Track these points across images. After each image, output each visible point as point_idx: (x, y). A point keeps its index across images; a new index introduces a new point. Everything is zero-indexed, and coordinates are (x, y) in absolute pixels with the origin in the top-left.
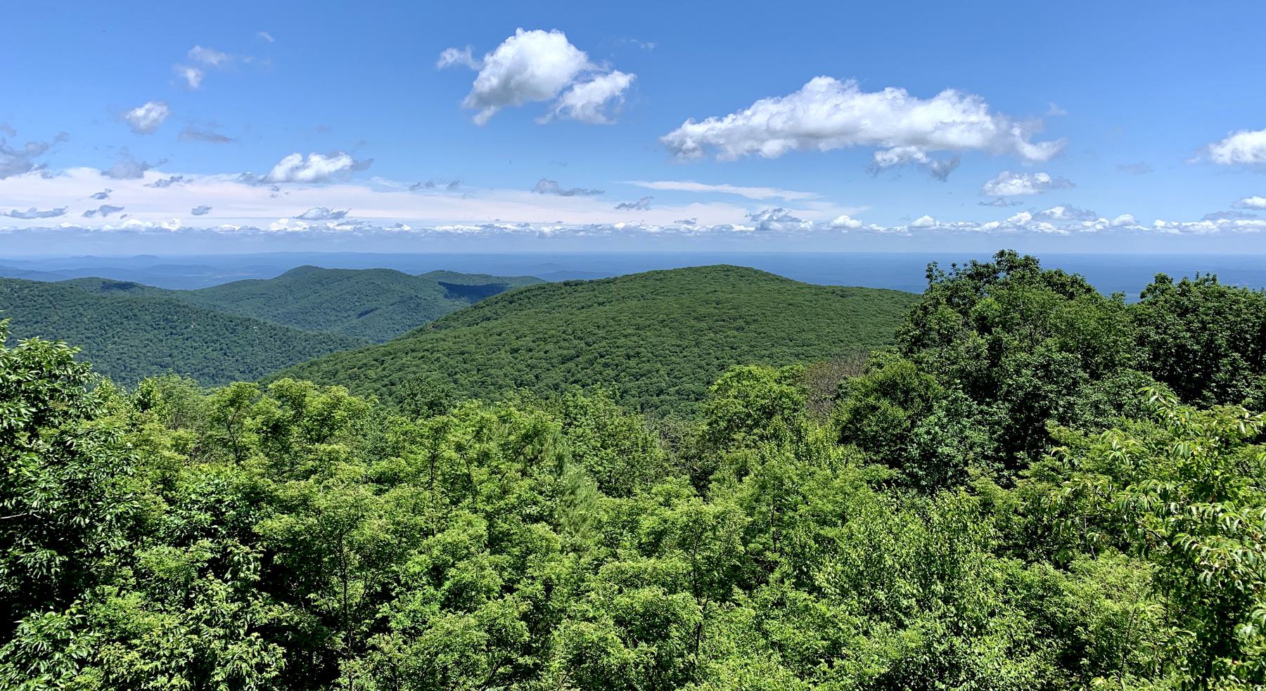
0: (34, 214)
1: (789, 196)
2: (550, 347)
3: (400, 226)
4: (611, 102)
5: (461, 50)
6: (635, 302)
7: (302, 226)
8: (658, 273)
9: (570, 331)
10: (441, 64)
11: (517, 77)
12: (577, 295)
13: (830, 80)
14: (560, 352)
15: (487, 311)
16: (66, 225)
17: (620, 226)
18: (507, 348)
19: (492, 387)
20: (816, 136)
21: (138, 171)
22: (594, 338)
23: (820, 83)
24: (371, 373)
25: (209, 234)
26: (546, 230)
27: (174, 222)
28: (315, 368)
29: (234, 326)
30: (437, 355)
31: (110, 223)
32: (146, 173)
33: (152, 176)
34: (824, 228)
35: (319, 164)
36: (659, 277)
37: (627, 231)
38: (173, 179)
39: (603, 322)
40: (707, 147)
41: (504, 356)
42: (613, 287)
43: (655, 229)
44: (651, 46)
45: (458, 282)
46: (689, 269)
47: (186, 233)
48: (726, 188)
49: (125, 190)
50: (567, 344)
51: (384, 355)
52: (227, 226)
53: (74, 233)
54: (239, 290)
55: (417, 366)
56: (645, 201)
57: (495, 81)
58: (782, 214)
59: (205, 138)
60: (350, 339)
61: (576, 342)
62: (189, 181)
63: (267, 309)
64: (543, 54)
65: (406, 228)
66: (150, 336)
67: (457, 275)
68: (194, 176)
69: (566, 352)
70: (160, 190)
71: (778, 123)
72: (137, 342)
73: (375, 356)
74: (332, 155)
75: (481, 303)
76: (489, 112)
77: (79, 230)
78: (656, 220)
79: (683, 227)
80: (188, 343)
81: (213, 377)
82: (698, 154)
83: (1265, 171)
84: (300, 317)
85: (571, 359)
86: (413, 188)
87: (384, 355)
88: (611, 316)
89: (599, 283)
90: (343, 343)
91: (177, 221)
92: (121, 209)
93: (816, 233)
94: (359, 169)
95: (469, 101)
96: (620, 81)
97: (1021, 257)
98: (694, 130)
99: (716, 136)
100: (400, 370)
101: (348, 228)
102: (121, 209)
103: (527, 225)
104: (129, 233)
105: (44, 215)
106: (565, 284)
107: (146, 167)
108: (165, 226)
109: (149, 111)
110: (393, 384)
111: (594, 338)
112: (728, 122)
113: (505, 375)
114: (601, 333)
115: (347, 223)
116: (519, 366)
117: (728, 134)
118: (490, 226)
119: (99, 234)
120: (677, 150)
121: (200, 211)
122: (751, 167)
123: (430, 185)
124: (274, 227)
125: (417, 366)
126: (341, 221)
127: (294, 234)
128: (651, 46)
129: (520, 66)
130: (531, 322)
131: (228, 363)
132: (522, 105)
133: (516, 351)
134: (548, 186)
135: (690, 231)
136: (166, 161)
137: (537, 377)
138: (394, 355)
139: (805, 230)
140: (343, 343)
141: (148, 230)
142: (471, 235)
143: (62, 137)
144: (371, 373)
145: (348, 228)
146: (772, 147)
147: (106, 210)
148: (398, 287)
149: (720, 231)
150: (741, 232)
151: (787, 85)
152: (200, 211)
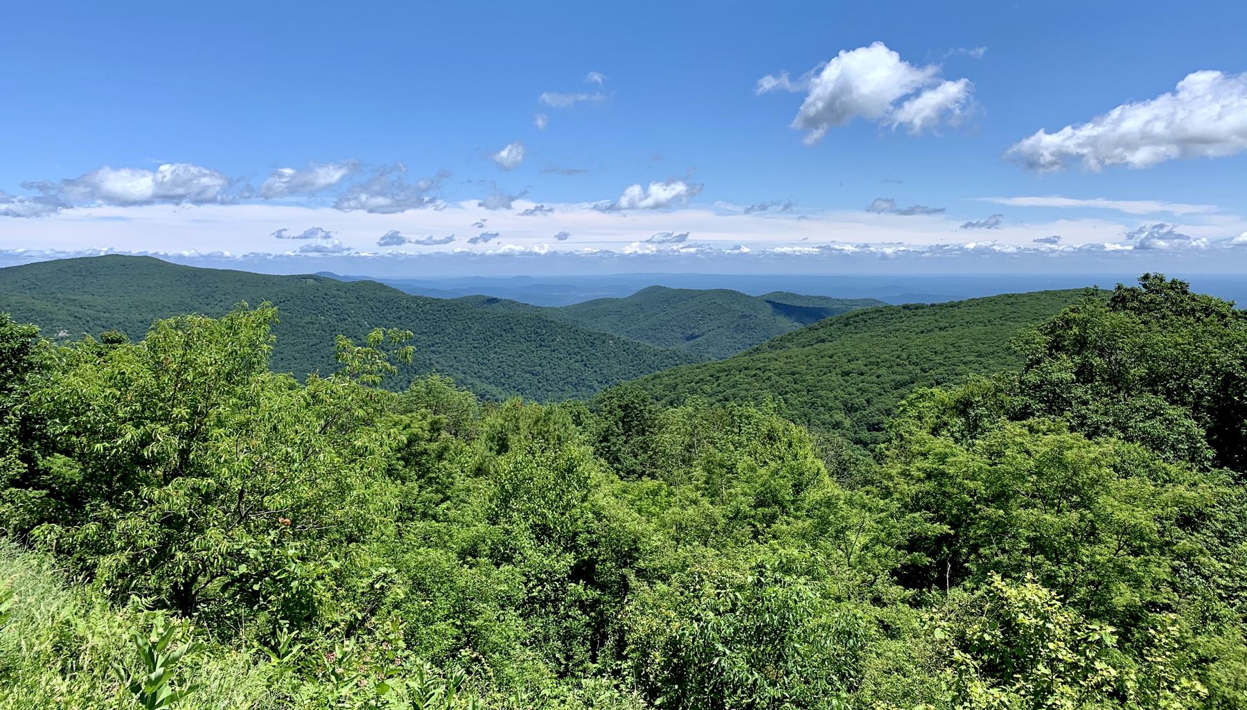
0: (430, 242)
1: (1180, 209)
2: (882, 371)
3: (738, 247)
4: (944, 113)
5: (776, 75)
6: (981, 327)
7: (652, 249)
8: (1009, 296)
9: (905, 356)
10: (760, 90)
11: (843, 99)
12: (916, 318)
13: (1217, 74)
14: (893, 377)
15: (821, 333)
16: (458, 250)
17: (971, 246)
18: (838, 370)
19: (822, 409)
20: (1204, 141)
21: (507, 203)
22: (930, 364)
23: (1200, 81)
24: (707, 388)
25: (571, 258)
26: (888, 251)
27: (543, 247)
28: (658, 381)
29: (594, 340)
30: (768, 374)
31: (490, 248)
32: (513, 204)
33: (521, 205)
34: (1224, 245)
35: (659, 192)
36: (1011, 300)
37: (979, 252)
38: (537, 209)
39: (940, 348)
40: (1065, 159)
41: (835, 378)
42: (957, 311)
43: (1012, 249)
44: (981, 51)
45: (797, 303)
46: (1046, 292)
47: (553, 256)
48: (1101, 203)
49: (497, 219)
50: (900, 369)
51: (719, 372)
52: (587, 250)
53: (464, 257)
54: (598, 308)
55: (749, 383)
56: (993, 222)
57: (820, 105)
58: (1165, 230)
59: (568, 169)
60: (694, 356)
61: (911, 367)
62: (551, 210)
63: (621, 325)
64: (871, 70)
65: (745, 250)
66: (524, 347)
67: (795, 296)
68: (553, 206)
69: (899, 377)
70: (529, 217)
71: (1159, 128)
72: (513, 353)
73: (711, 372)
74: (669, 182)
75: (816, 324)
76: (817, 134)
77: (468, 254)
78: (1010, 239)
79: (1046, 247)
80: (555, 354)
81: (575, 386)
82: (1056, 168)
83: (1193, 165)
84: (650, 333)
85: (904, 384)
86: (747, 211)
87: (719, 372)
88: (950, 341)
89: (941, 306)
90: (688, 359)
91: (546, 246)
92: (497, 235)
93: (1213, 250)
94: (696, 195)
95: (797, 123)
96: (952, 90)
97: (1168, 280)
98: (1048, 142)
99: (1079, 145)
100: (734, 386)
101: (692, 250)
102: (497, 235)
103: (867, 246)
104: (507, 257)
105: (440, 242)
106: (905, 307)
107: (512, 199)
108: (536, 249)
109: (510, 151)
110: (727, 400)
111: (930, 364)
112: (1088, 131)
113: (836, 398)
114: (939, 359)
115: (690, 246)
116: (850, 389)
117: (1092, 142)
118: (827, 248)
119: (484, 258)
120: (1032, 162)
121: (562, 236)
122: (1110, 177)
123: (763, 207)
124: (628, 250)
125: (749, 383)
126: (685, 244)
127: (643, 255)
128: (981, 51)
129: (844, 88)
130: (865, 346)
131: (588, 373)
132: (849, 123)
133: (847, 374)
134: (884, 205)
135: (1054, 251)
136: (526, 192)
137: (868, 401)
138: (727, 371)
139: (1197, 248)
140: (688, 359)
141: (522, 253)
142: (810, 258)
143: (443, 174)
144: (707, 388)
145: (692, 250)
146: (1141, 156)
147: (486, 237)
148: (738, 307)
149: (1089, 251)
150: (1116, 251)
151: (1162, 82)
152: (562, 236)
